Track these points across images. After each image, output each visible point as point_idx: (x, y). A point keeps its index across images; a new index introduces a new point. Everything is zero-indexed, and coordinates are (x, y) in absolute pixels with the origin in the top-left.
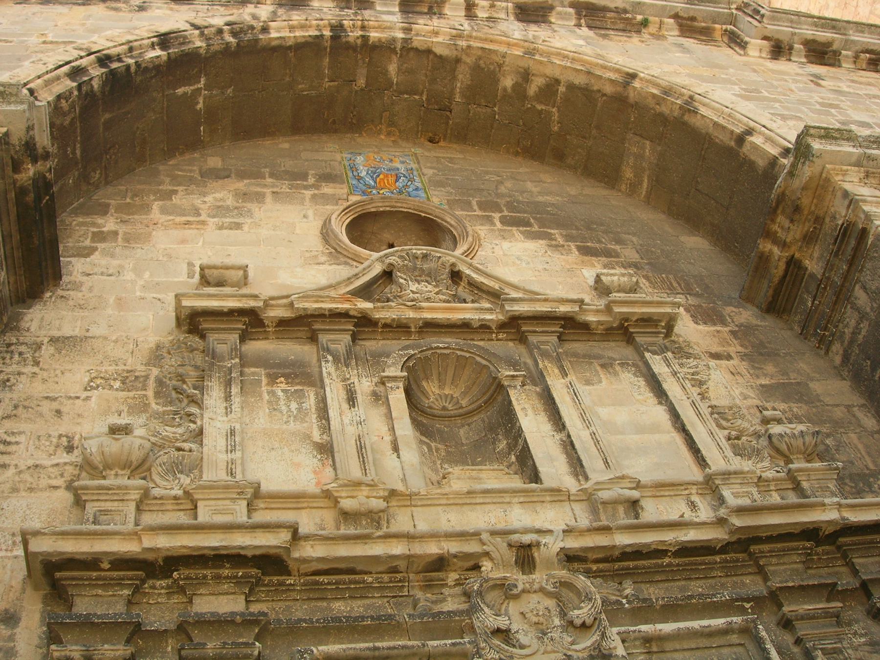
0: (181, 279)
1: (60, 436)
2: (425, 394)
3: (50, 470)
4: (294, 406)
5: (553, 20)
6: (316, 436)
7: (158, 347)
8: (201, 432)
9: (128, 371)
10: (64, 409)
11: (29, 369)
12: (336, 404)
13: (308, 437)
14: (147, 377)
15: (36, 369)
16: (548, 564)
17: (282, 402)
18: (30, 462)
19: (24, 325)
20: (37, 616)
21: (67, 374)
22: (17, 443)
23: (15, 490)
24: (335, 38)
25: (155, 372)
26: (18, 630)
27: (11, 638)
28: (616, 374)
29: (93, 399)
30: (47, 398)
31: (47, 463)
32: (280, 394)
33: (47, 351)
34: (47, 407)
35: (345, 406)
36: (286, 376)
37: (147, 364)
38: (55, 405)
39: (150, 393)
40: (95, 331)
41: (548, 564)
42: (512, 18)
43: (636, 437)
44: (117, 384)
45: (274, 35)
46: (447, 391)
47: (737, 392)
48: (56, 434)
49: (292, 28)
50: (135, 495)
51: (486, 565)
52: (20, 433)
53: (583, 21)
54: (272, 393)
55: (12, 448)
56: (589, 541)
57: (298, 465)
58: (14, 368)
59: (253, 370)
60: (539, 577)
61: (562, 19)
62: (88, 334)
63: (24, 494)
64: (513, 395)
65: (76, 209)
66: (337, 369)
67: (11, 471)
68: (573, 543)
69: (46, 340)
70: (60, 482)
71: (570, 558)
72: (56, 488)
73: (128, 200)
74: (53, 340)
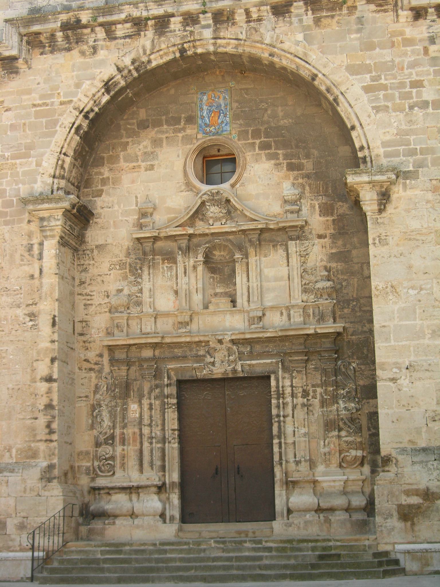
0: (132, 208)
1: (105, 291)
2: (215, 255)
3: (104, 305)
4: (169, 274)
5: (292, 10)
6: (175, 289)
7: (128, 249)
8: (142, 289)
9: (121, 261)
10: (104, 280)
11: (92, 262)
12: (180, 275)
13: (173, 288)
14: (126, 263)
15: (93, 262)
16: (226, 343)
17: (166, 272)
18: (98, 303)
19: (86, 240)
20: (107, 354)
21: (103, 264)
22: (94, 295)
23: (96, 314)
24: (182, 56)
25: (128, 260)
26: (103, 359)
27: (102, 361)
28: (277, 251)
29: (112, 274)
30: (99, 275)
31: (103, 303)
32: (165, 268)
33: (96, 252)
34: (99, 279)
35: (183, 275)
36: (167, 259)
37: (126, 257)
38: (101, 278)
39: (128, 271)
40: (110, 241)
41: (226, 343)
42: (270, 14)
43: (273, 283)
44: (118, 267)
45: (154, 64)
46: (222, 253)
47: (320, 258)
48: (103, 291)
49: (161, 57)
50: (126, 318)
51: (211, 343)
52: (94, 291)
53: (309, 8)
54: (163, 268)
55: (93, 297)
56: (238, 337)
57: (169, 299)
58: (87, 262)
59: (158, 257)
60: (223, 346)
61: (298, 9)
62: (107, 243)
63: (98, 315)
64: (237, 264)
65: (93, 162)
66: (182, 257)
67: (94, 307)
68: (234, 337)
69: (94, 247)
70: (107, 310)
71: (233, 342)
72: (106, 312)
73: (111, 153)
74: (97, 247)
